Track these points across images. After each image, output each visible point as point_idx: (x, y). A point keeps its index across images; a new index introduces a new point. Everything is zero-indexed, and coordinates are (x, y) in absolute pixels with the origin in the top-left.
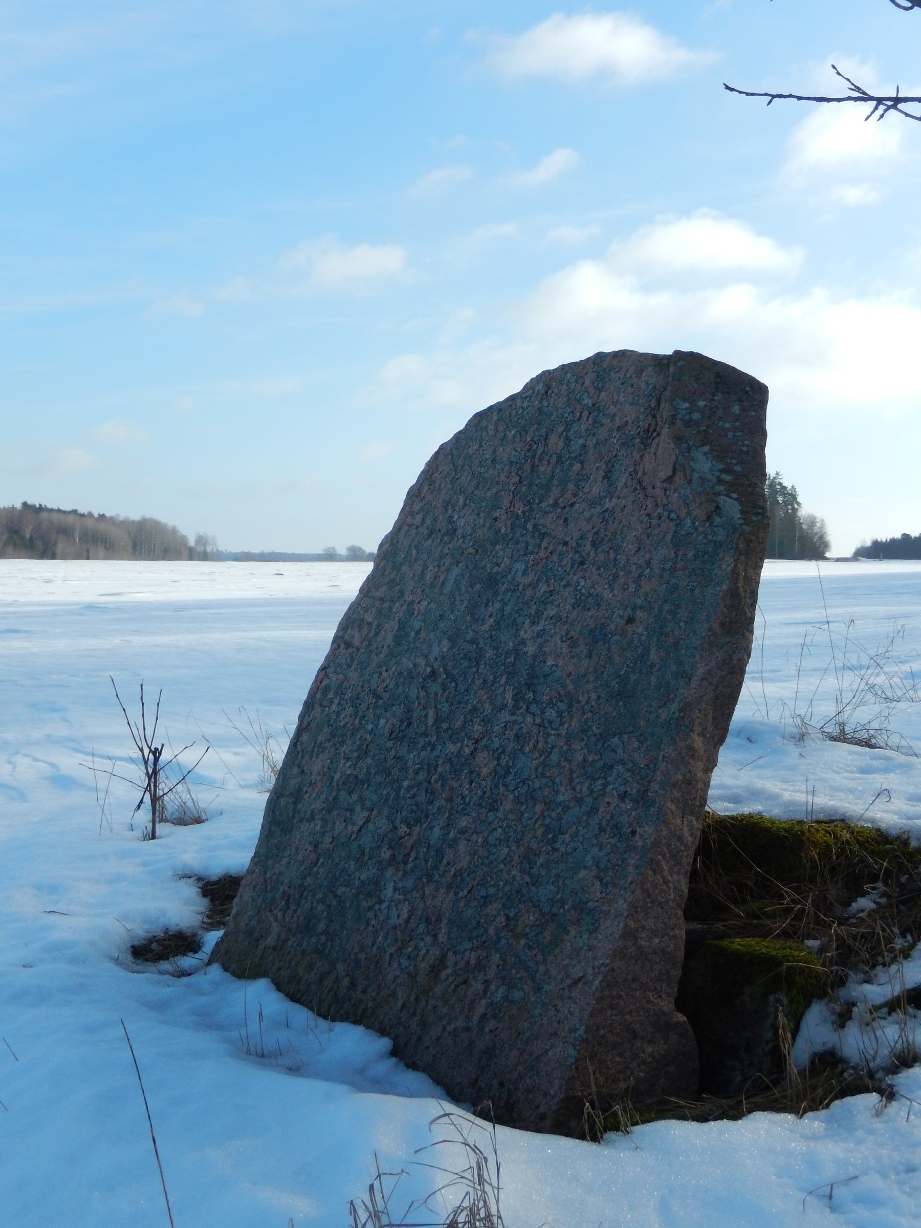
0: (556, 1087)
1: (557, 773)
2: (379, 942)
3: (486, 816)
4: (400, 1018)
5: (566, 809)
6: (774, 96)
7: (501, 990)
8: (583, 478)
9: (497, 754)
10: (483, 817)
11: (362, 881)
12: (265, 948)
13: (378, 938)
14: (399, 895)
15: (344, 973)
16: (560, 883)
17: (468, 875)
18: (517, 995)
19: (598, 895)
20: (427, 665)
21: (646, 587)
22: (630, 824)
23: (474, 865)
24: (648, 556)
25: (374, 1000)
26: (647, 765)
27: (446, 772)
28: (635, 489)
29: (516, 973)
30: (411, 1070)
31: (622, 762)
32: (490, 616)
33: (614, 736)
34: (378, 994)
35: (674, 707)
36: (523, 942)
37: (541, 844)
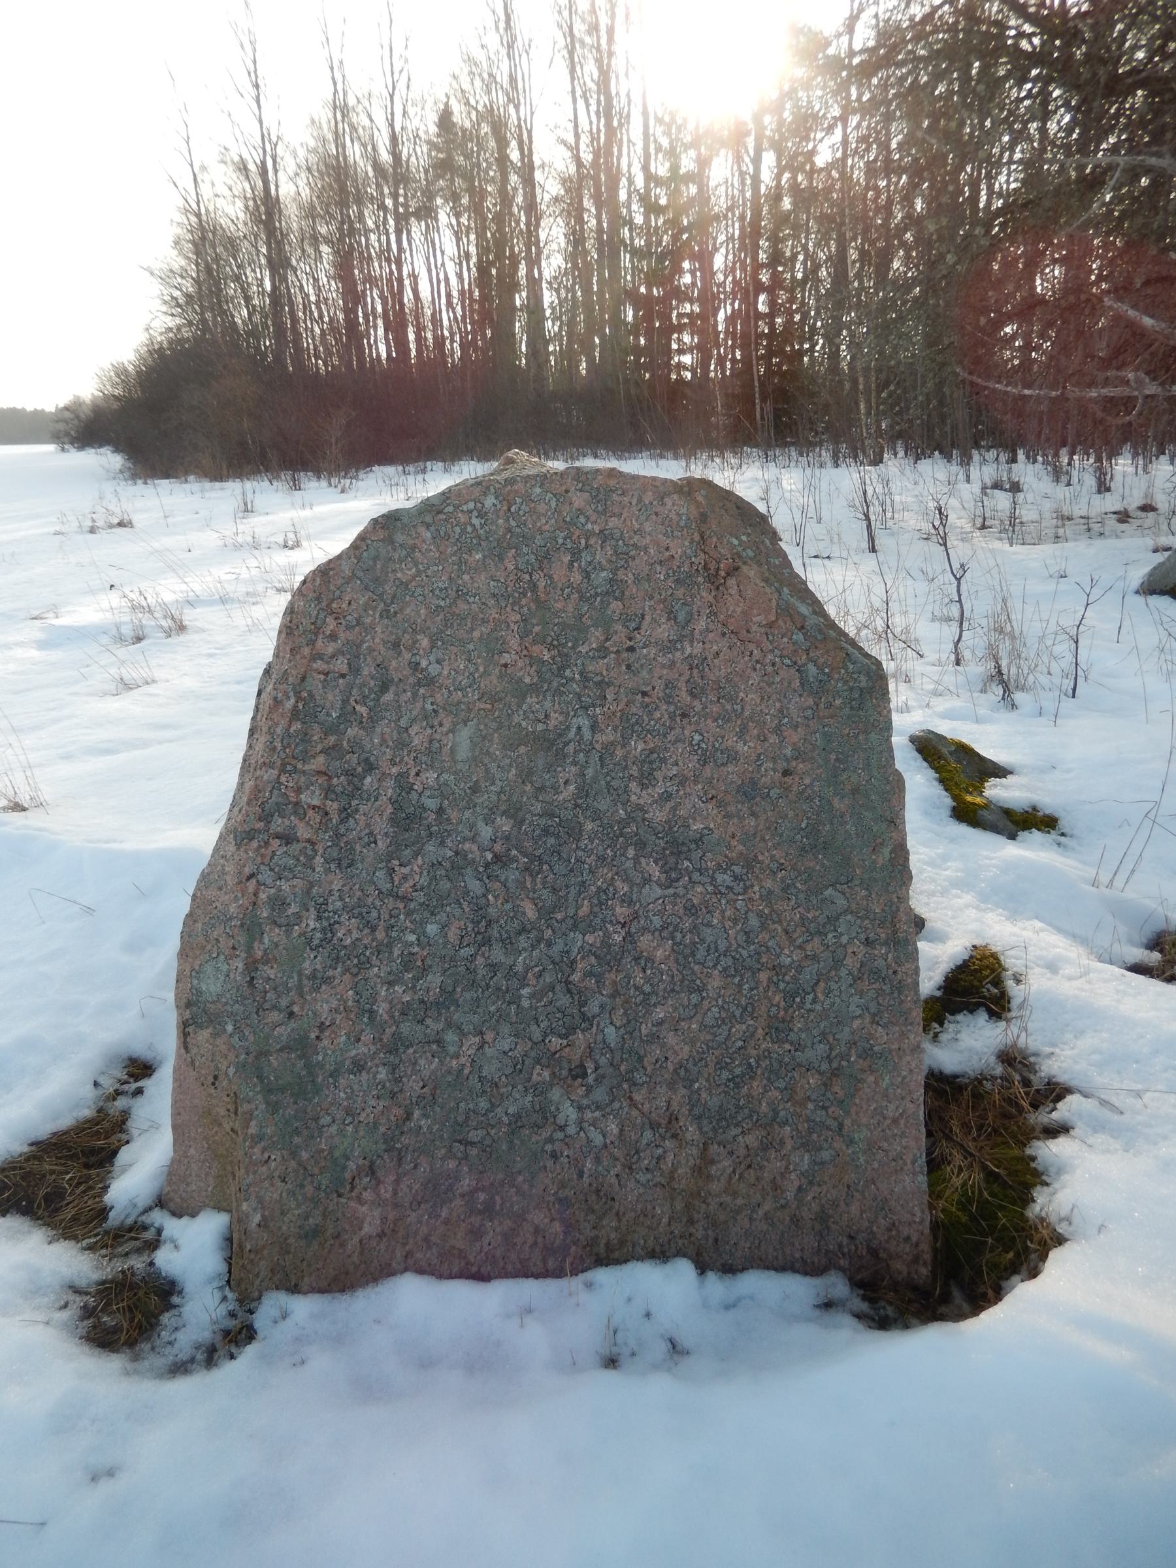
0: (919, 1214)
1: (767, 937)
2: (590, 1170)
3: (689, 999)
4: (672, 1233)
5: (800, 969)
6: (1077, 642)
7: (806, 1157)
8: (635, 623)
9: (667, 930)
10: (686, 1002)
11: (513, 1116)
12: (361, 1241)
13: (584, 1166)
14: (593, 1112)
15: (547, 1220)
16: (831, 1039)
17: (695, 1065)
18: (826, 1155)
19: (885, 1038)
20: (482, 850)
21: (795, 737)
22: (888, 967)
23: (698, 1052)
24: (778, 705)
25: (617, 1229)
26: (883, 910)
27: (592, 966)
28: (724, 634)
29: (819, 1136)
30: (164, 1274)
31: (847, 911)
32: (566, 782)
33: (827, 888)
34: (619, 1220)
35: (886, 851)
36: (810, 1106)
37: (791, 1010)
